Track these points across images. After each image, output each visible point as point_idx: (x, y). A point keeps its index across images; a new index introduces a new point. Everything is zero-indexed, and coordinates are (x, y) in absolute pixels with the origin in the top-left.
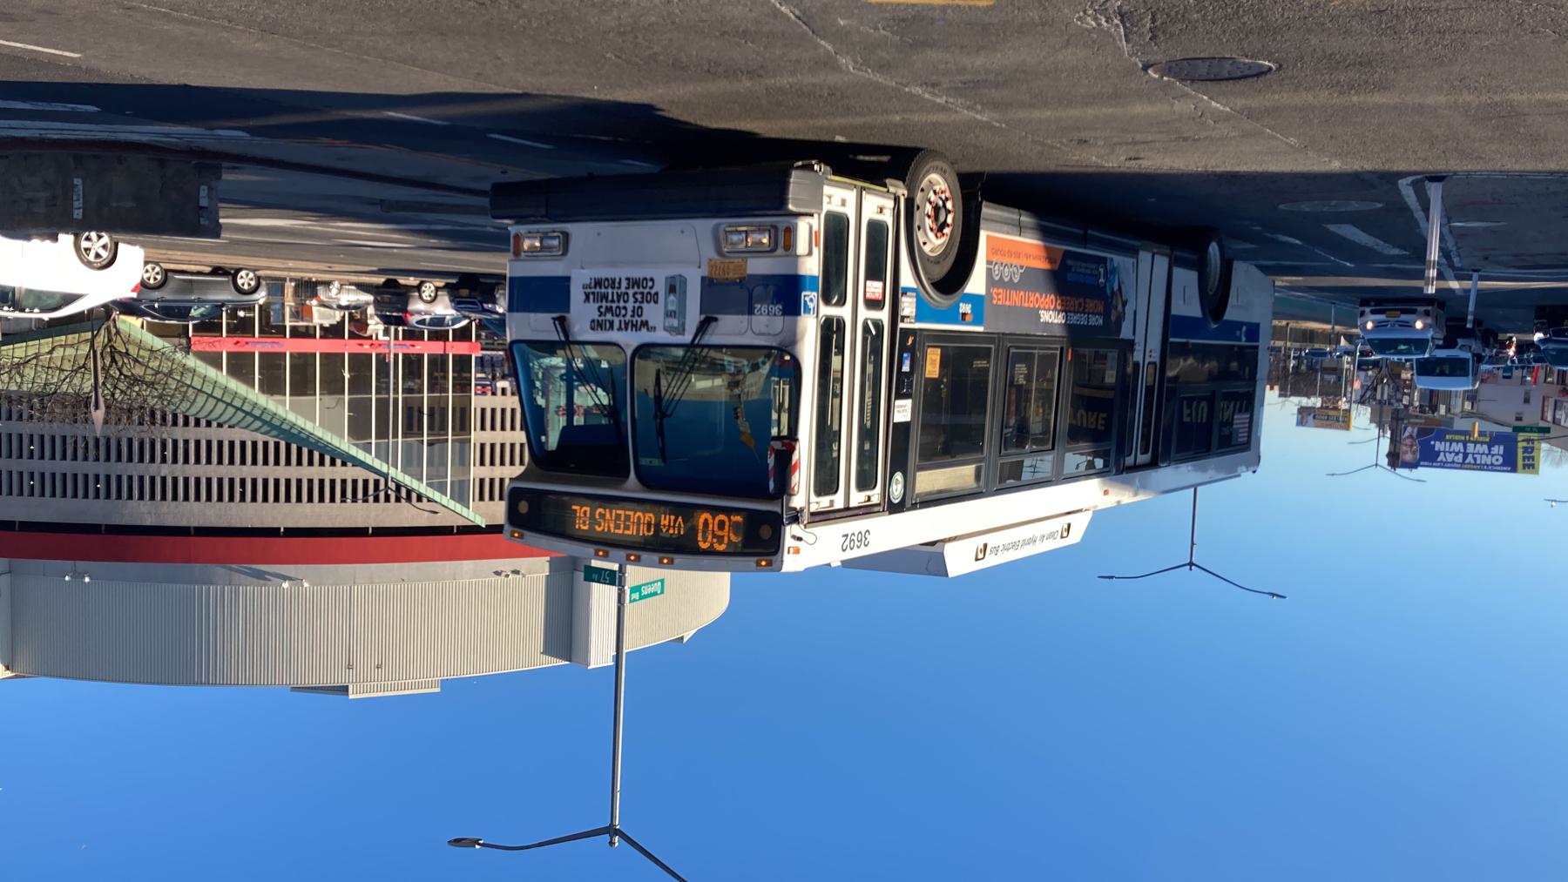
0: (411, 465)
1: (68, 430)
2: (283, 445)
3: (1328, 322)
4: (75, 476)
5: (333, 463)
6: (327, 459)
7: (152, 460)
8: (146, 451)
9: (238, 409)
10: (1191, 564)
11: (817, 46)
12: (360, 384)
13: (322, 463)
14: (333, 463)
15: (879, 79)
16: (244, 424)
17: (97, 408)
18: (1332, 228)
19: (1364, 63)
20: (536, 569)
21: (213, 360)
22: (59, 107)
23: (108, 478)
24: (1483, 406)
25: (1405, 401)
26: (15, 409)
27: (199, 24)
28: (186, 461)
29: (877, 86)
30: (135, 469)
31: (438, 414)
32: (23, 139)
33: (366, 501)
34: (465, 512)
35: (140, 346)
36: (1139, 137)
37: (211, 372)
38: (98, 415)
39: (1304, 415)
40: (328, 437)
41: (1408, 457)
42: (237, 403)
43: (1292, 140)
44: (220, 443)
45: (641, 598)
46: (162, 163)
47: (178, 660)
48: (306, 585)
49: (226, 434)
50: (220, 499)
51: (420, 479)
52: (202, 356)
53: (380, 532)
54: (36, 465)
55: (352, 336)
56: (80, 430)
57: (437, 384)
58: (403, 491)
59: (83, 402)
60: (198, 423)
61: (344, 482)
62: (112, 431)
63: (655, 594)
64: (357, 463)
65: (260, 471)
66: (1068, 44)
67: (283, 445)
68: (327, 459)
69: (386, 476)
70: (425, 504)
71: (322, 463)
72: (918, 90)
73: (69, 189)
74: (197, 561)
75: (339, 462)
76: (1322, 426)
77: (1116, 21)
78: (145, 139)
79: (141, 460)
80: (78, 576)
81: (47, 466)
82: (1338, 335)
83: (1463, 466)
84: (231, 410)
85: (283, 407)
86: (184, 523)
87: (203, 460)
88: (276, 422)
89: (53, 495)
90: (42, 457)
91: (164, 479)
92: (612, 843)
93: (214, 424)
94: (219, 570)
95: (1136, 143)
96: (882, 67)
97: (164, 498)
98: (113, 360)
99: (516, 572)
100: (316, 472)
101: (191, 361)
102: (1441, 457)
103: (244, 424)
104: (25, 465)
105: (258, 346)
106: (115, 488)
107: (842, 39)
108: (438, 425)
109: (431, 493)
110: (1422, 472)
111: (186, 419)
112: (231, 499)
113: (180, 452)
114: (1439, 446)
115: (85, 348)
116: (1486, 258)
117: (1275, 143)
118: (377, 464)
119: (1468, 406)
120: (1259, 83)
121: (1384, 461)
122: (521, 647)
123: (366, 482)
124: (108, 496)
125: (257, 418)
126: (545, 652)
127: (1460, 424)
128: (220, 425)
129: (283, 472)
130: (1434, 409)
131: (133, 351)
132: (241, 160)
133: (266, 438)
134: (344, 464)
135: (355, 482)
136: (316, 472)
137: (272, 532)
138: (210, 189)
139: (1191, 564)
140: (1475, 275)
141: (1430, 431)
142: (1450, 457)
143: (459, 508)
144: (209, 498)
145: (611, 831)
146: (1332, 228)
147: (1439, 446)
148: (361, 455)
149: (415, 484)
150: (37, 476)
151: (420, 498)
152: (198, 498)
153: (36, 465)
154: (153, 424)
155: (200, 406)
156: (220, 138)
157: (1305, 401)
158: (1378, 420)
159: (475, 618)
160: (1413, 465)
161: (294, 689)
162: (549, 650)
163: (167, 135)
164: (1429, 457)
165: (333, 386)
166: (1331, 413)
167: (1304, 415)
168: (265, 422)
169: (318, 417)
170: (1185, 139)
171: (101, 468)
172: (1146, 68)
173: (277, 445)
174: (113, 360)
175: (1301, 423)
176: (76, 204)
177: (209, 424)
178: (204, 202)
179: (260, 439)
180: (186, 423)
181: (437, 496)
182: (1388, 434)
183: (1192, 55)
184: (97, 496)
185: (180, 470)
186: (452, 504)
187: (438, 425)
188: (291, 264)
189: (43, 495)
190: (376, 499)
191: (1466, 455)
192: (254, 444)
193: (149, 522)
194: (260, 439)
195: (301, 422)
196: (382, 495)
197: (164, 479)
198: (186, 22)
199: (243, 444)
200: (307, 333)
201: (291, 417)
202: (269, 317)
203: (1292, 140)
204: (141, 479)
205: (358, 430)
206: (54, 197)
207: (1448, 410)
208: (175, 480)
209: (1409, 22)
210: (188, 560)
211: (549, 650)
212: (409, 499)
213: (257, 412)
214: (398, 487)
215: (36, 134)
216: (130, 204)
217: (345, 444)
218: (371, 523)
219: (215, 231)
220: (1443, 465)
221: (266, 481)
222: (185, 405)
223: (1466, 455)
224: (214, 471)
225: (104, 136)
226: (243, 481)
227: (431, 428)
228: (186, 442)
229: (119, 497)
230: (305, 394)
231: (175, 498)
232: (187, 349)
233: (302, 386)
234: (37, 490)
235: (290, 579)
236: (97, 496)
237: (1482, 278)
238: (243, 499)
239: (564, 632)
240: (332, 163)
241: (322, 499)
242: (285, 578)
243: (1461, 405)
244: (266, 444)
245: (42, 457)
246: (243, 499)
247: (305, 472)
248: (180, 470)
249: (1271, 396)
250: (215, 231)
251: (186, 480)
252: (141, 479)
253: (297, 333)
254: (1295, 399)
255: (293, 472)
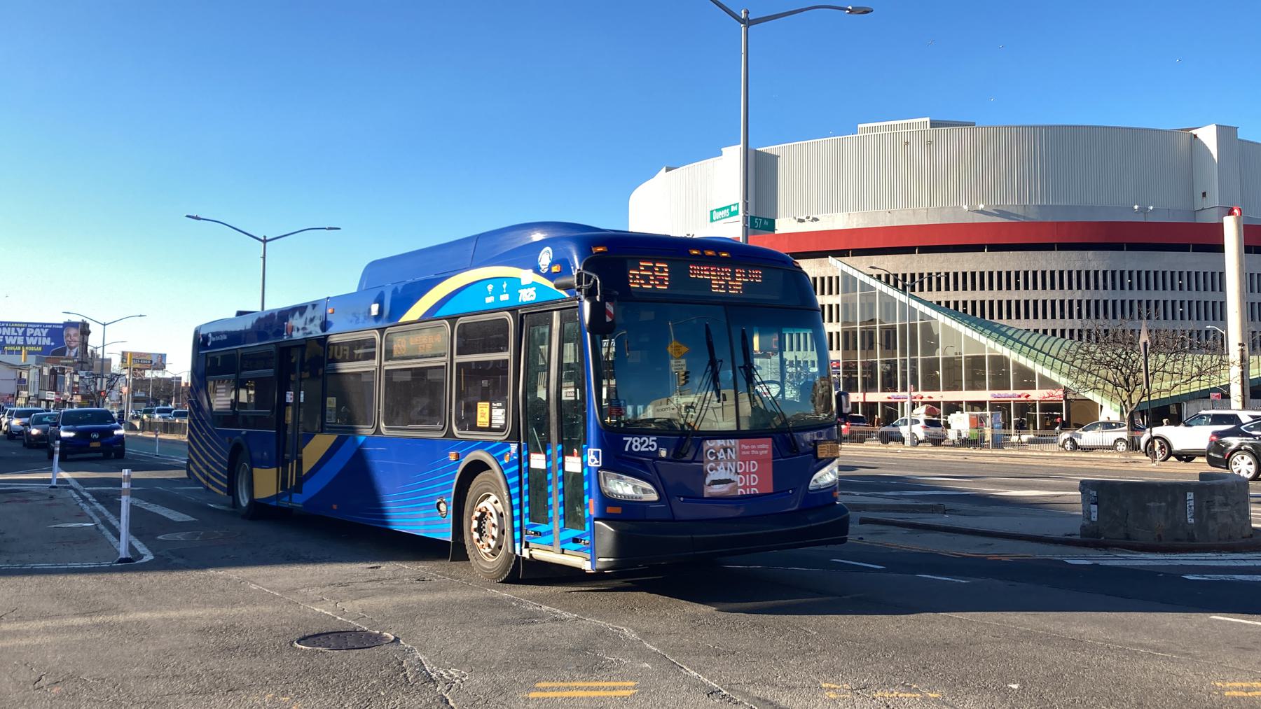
0: (889, 303)
1: (1163, 325)
2: (987, 317)
3: (161, 440)
4: (1147, 288)
5: (947, 303)
6: (952, 307)
7: (1088, 302)
8: (1094, 309)
9: (1033, 348)
10: (265, 241)
11: (659, 646)
12: (931, 366)
13: (956, 303)
14: (947, 303)
15: (602, 623)
16: (1020, 333)
17: (1145, 344)
18: (188, 518)
19: (228, 650)
20: (785, 225)
21: (1047, 383)
22: (1214, 577)
23: (1122, 288)
24: (13, 375)
25: (76, 379)
26: (1195, 340)
27: (1131, 645)
28: (1062, 302)
29: (600, 617)
30: (1102, 295)
31: (889, 344)
32: (1234, 552)
33: (930, 274)
34: (845, 268)
35: (1104, 392)
36: (379, 585)
37: (1047, 373)
38: (1144, 338)
39: (159, 362)
40: (955, 325)
41: (73, 331)
42: (1026, 349)
43: (253, 587)
44: (1036, 317)
45: (729, 207)
46: (1128, 537)
47: (1061, 146)
48: (965, 207)
49: (1032, 324)
50: (1035, 273)
51: (881, 292)
52: (1054, 385)
53: (909, 250)
54: (1178, 296)
55: (937, 404)
56: (1154, 324)
57: (870, 368)
58: (892, 282)
59: (1155, 347)
60: (1054, 332)
61: (939, 289)
62: (1129, 325)
63: (718, 210)
64: (928, 304)
65: (1004, 295)
66: (466, 655)
67: (987, 317)
68: (952, 307)
69: (911, 296)
70: (875, 272)
71: (956, 303)
72: (567, 615)
73: (1197, 515)
74: (1052, 223)
75: (943, 305)
76: (145, 354)
77: (434, 675)
78: (1142, 555)
79: (1097, 302)
80: (1143, 210)
81: (1169, 296)
82: (142, 430)
83: (27, 326)
84: (1031, 343)
85: (991, 347)
86: (1063, 253)
87: (1101, 304)
88: (995, 335)
89: (1164, 273)
90: (1173, 302)
91: (1079, 287)
92: (747, 12)
93: (1041, 332)
94: (1034, 217)
95: (378, 580)
96: (602, 633)
97: (1079, 273)
98: (1127, 380)
99: (801, 221)
100: (961, 296)
101: (1064, 381)
102: (45, 332)
103: (1020, 333)
104: (1185, 296)
105: (1012, 394)
106: (1116, 279)
107: (645, 655)
108: (869, 337)
109: (873, 283)
110: (60, 319)
111: (1063, 335)
112: (1026, 273)
113: (1066, 309)
114: (47, 341)
115: (1155, 386)
116: (52, 497)
117: (268, 584)
118: (914, 304)
119: (25, 375)
120: (302, 632)
121: (93, 327)
122: (797, 162)
123: (921, 289)
124: (1122, 273)
125: (1010, 337)
126: (776, 157)
127: (32, 360)
128: (1036, 331)
129: (987, 295)
130: (53, 372)
131: (1110, 387)
132: (1067, 542)
133: (1001, 322)
134: (939, 303)
135: (930, 289)
136: (961, 296)
137: (994, 248)
138: (1089, 519)
139: (265, 241)
140: (54, 484)
141: (54, 353)
142: (37, 332)
143: (850, 271)
144: (1044, 273)
145: (748, 23)
146: (188, 518)
147: (47, 341)
148: (928, 311)
149: (885, 288)
150: (1177, 287)
151: (879, 277)
152: (1052, 273)
153: (1178, 296)
154: (1080, 331)
155: (1055, 346)
156: (1086, 558)
157: (159, 374)
158: (106, 363)
159: (838, 185)
160: (69, 325)
161: (973, 124)
162: (773, 159)
163: (1126, 559)
164: (56, 332)
165: (952, 365)
166: (138, 366)
167: (159, 362)
168: (1004, 334)
169: (962, 340)
170: (340, 585)
171: (1128, 295)
172: (397, 640)
173: (992, 316)
174: (1127, 380)
175: (163, 357)
176: (1192, 503)
177: (1045, 332)
178: (1094, 508)
179: (1004, 321)
180: (1063, 332)
181: (867, 280)
182: (89, 348)
183: (366, 651)
184: (1130, 273)
185: (1067, 295)
186: (856, 274)
187: (869, 337)
188: (997, 460)
189: (1172, 273)
190: (921, 275)
191: (24, 334)
192: (1009, 317)
193: (1090, 253)
194: (1004, 321)
195: (976, 336)
196: (917, 279)
197: (1079, 287)
198: (1141, 645)
199: (1018, 317)
200: (973, 405)
201: (983, 339)
202: (1004, 417)
203: (253, 587)
204: (1096, 287)
205: (928, 329)
206: (1208, 508)
207: (41, 371)
208: (1070, 287)
209: (205, 681)
210: (1072, 225)
211: (773, 159)
212: (887, 277)
213: (1010, 342)
214: (896, 285)
215: (1224, 556)
216: (1152, 504)
217: (941, 319)
218: (916, 257)
219: (1085, 486)
220: (43, 326)
221: (1044, 287)
222: (1067, 345)
223: (24, 334)
224: (1040, 295)
225: (1173, 556)
226: (1017, 287)
227: (855, 333)
228: (1062, 317)
229: (1113, 273)
230: (973, 357)
231: (1070, 273)
232: (1066, 390)
233: (976, 363)
234: (1177, 276)
235: (978, 211)
236: (1130, 273)
237: (49, 481)
238: (1017, 274)
239: (760, 176)
240: (996, 541)
241: (956, 275)
242: (982, 212)
243: (31, 376)
244: (1000, 317)
245: (1173, 302)
246: (1017, 274)
247: (969, 296)
248: (1067, 295)
249: (186, 379)
250: (1085, 486)
251: (1062, 287)
252: (1096, 287)
253: (981, 405)
254: (168, 375)
255: (978, 295)
